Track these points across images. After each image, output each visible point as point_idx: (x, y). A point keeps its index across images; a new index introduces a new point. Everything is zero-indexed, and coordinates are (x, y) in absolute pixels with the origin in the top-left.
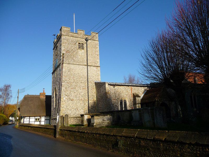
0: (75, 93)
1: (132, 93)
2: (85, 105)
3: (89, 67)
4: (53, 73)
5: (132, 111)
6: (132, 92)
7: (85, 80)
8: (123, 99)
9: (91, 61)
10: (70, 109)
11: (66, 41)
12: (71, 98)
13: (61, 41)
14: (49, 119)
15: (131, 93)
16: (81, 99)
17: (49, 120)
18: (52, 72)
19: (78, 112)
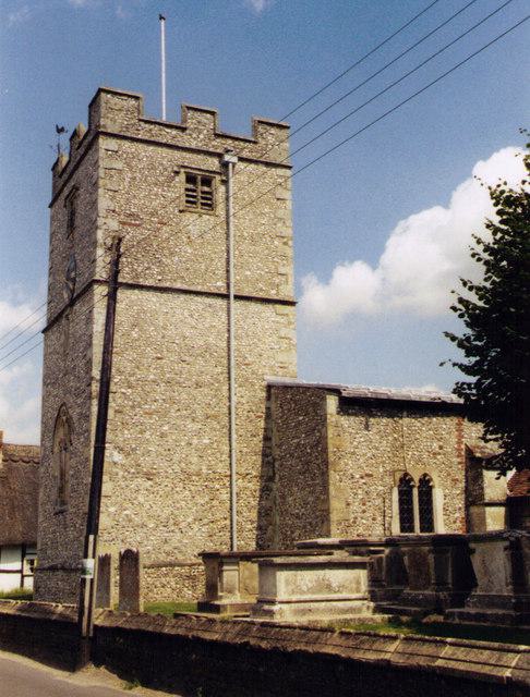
0: (163, 435)
1: (463, 446)
2: (215, 503)
3: (121, 294)
4: (51, 206)
5: (472, 545)
6: (460, 437)
7: (219, 370)
8: (416, 477)
9: (248, 273)
10: (137, 520)
11: (119, 165)
12: (146, 463)
13: (96, 164)
14: (19, 568)
15: (459, 443)
16: (197, 469)
17: (21, 571)
18: (49, 200)
19: (178, 535)
